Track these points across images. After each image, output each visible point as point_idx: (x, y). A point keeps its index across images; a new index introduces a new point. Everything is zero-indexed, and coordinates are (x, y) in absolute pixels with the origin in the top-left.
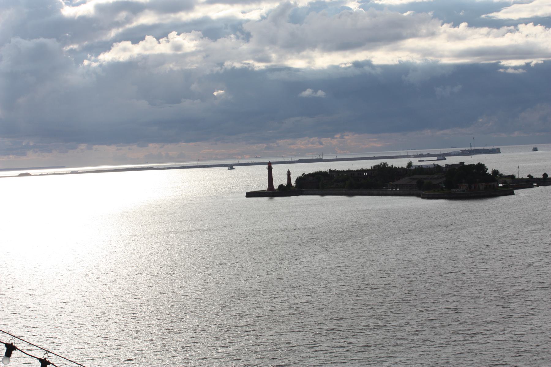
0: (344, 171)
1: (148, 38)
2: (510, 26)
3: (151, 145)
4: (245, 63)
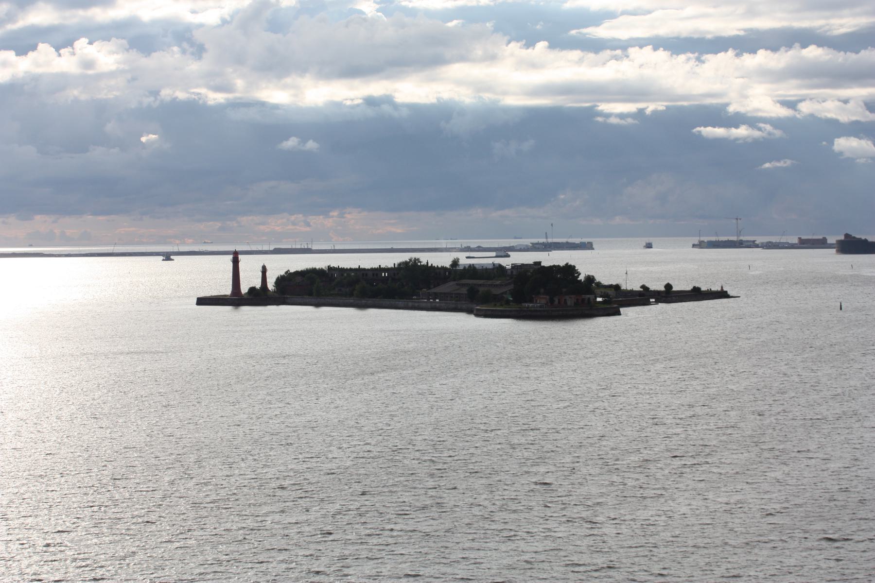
0: (351, 269)
2: (615, 50)
3: (38, 218)
4: (193, 93)
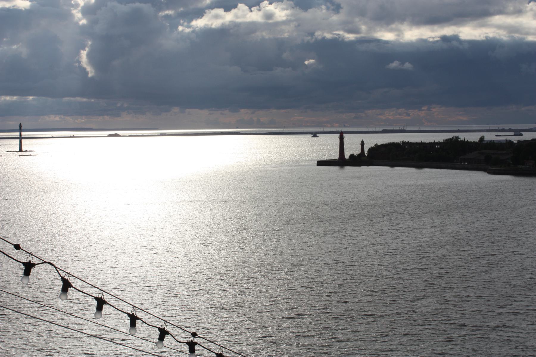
1: (240, 5)
3: (243, 111)
4: (335, 34)
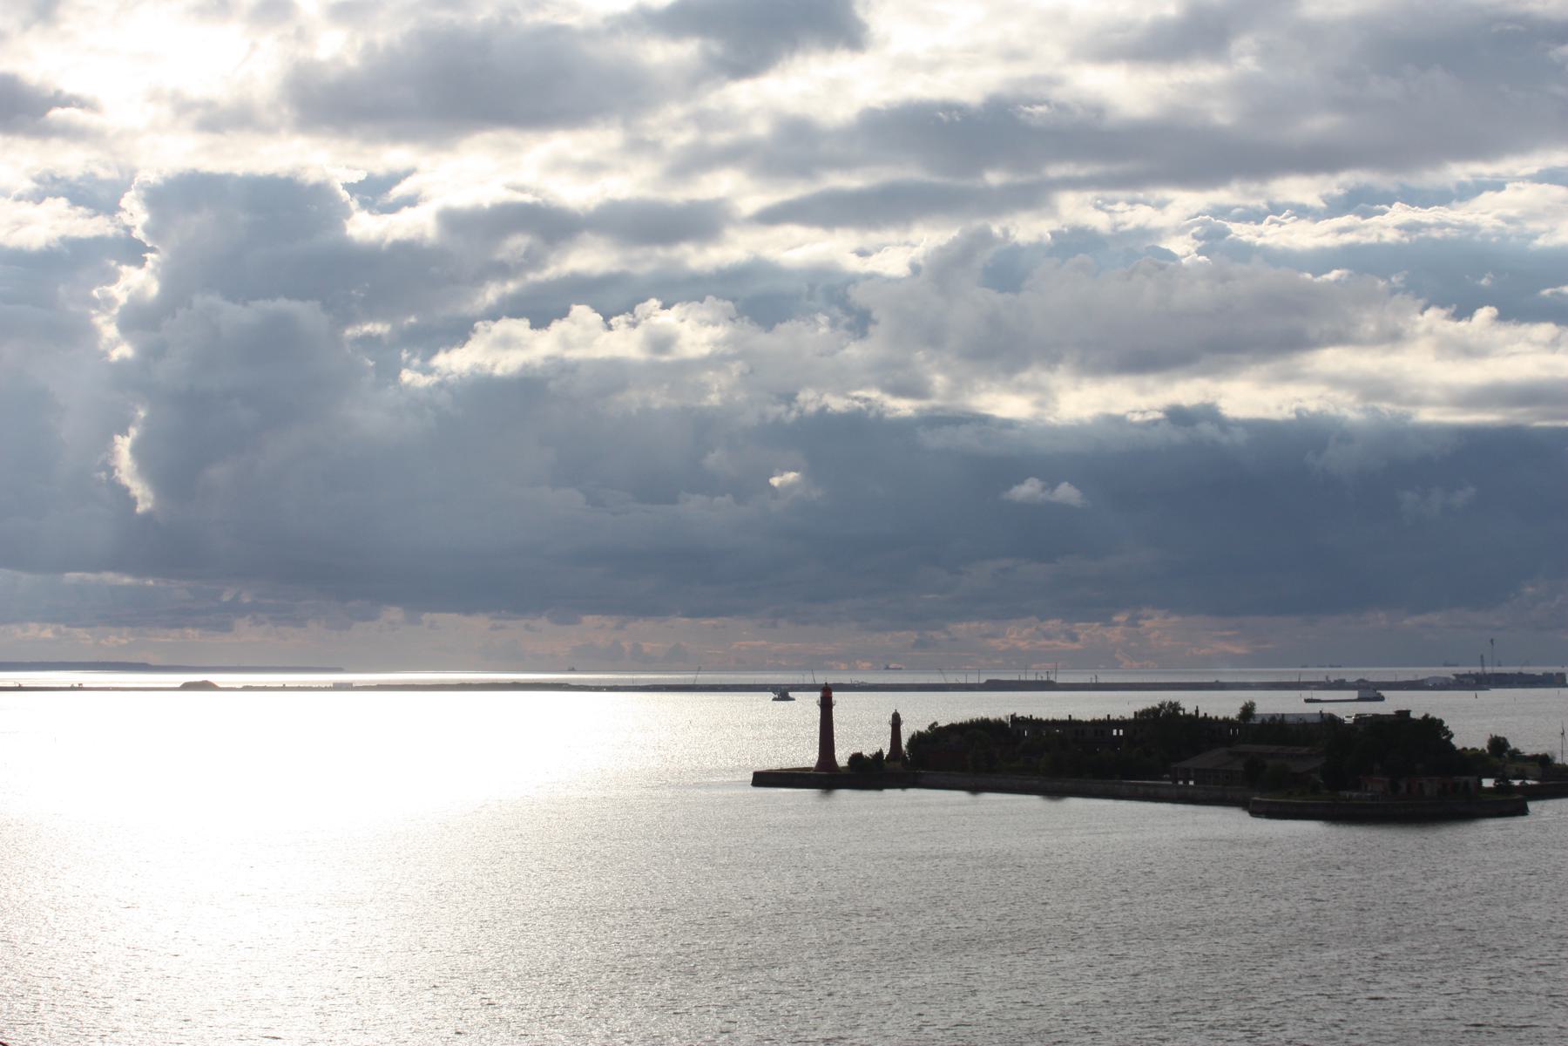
0: (1055, 723)
3: (588, 620)
4: (856, 398)
